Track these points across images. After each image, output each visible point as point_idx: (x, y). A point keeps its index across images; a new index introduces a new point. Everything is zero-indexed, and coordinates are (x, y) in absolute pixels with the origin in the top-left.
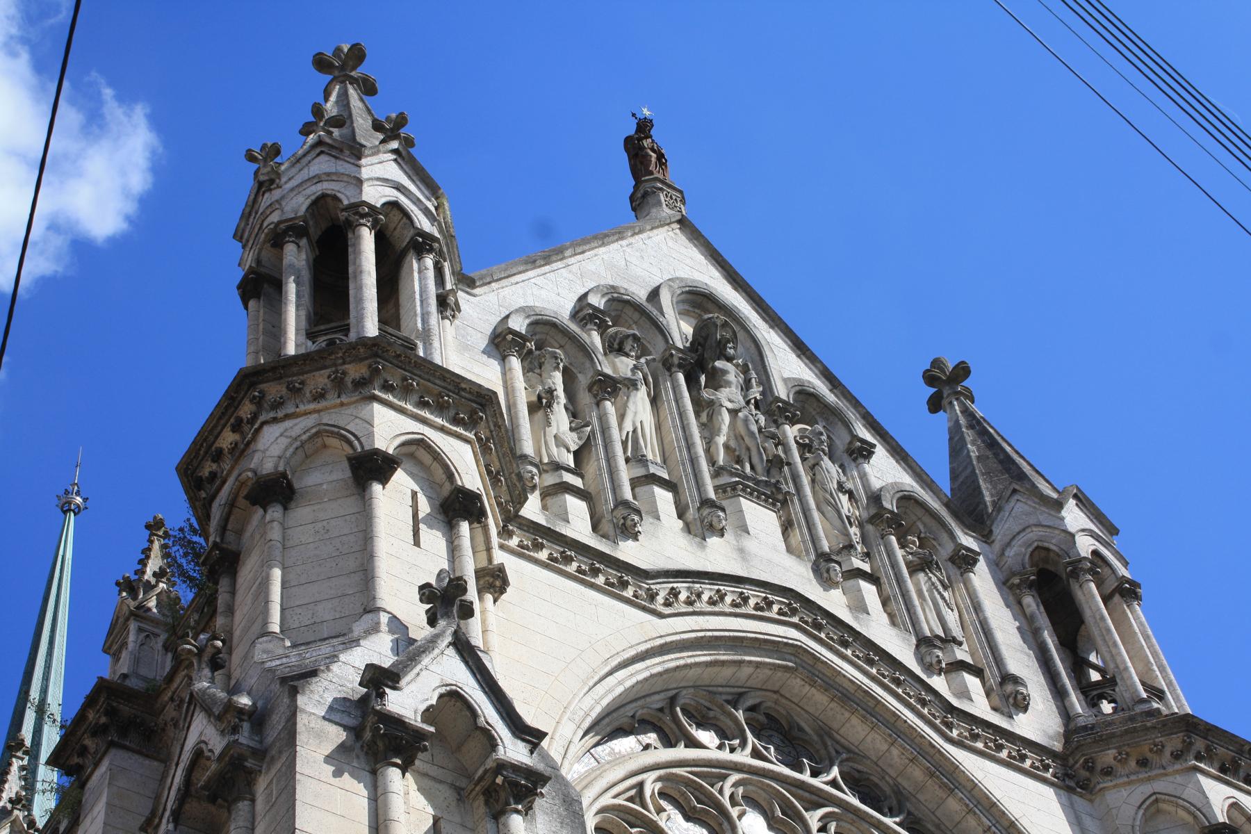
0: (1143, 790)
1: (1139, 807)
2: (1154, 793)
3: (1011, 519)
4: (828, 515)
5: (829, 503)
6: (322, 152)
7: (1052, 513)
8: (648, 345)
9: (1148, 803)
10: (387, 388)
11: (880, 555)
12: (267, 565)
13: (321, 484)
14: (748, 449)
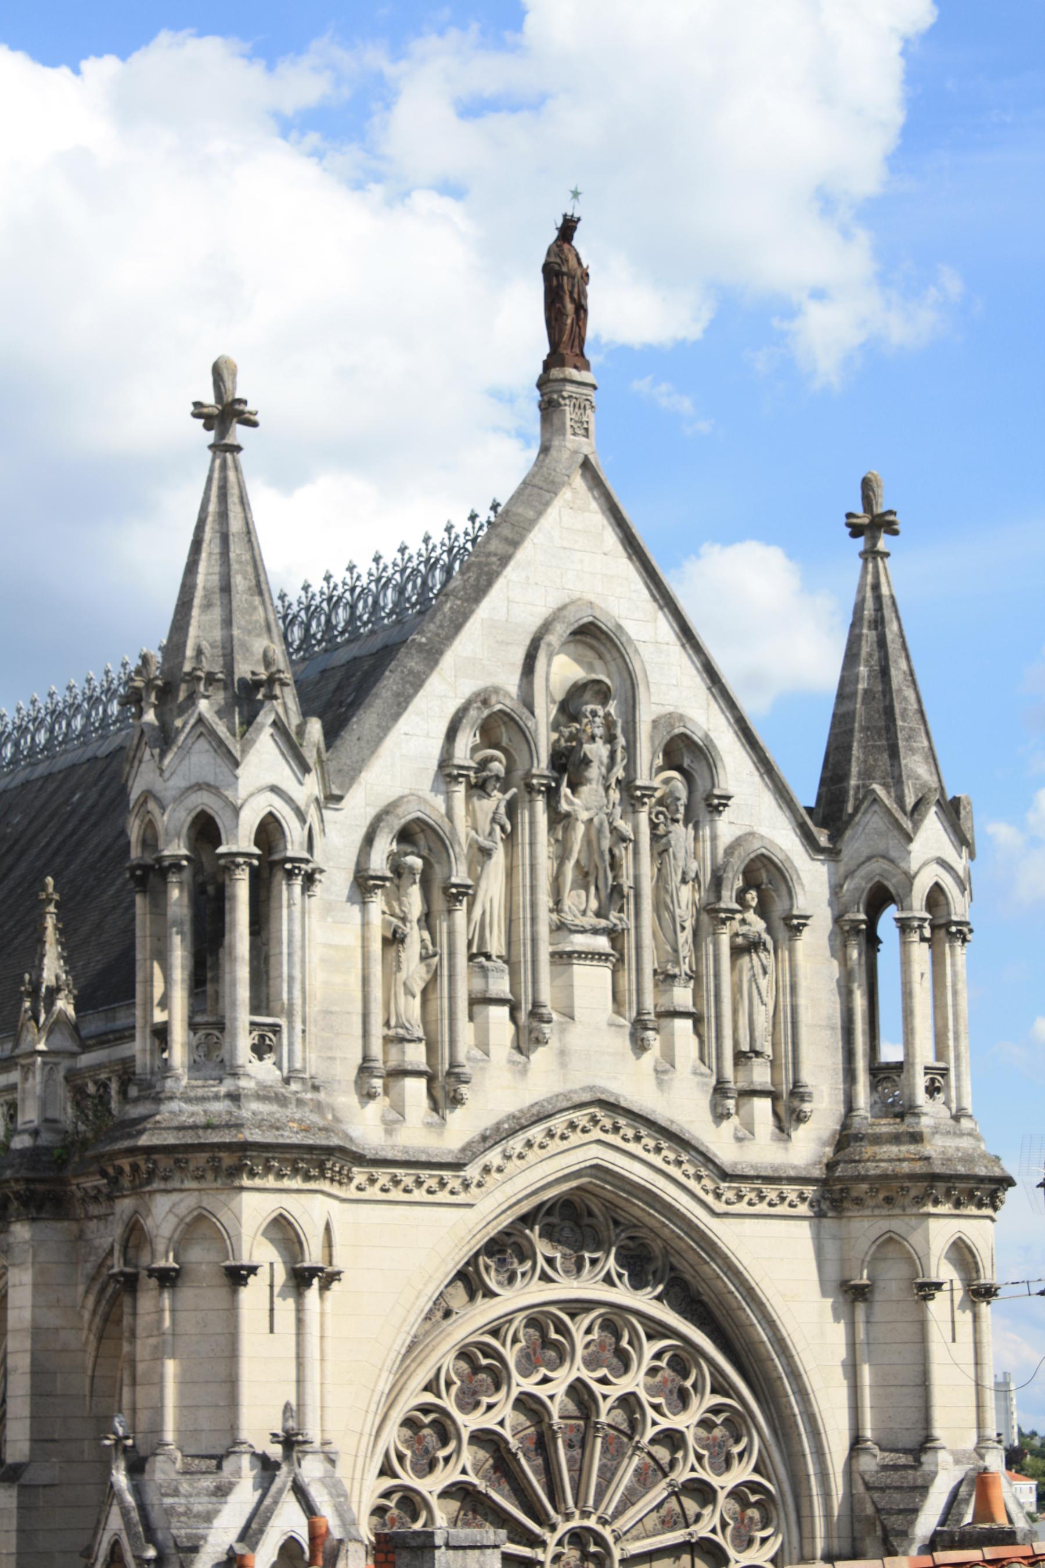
0: (883, 1225)
1: (874, 1242)
2: (890, 1231)
3: (863, 836)
4: (664, 924)
5: (667, 908)
6: (201, 734)
7: (902, 841)
8: (514, 753)
9: (881, 1240)
10: (252, 1174)
11: (707, 959)
12: (158, 1356)
13: (201, 1263)
14: (596, 867)
